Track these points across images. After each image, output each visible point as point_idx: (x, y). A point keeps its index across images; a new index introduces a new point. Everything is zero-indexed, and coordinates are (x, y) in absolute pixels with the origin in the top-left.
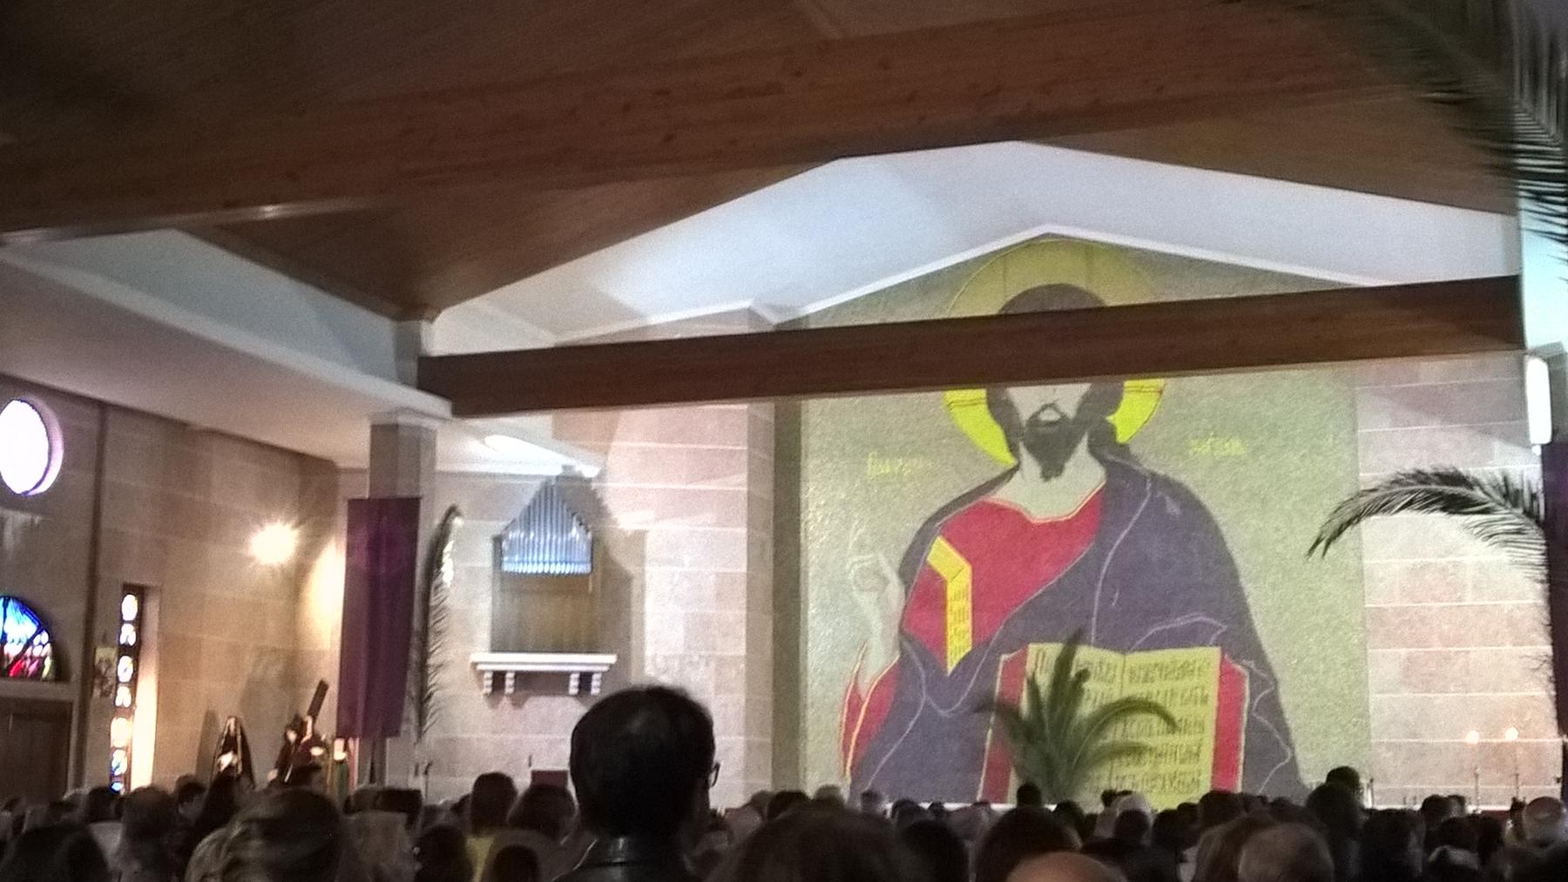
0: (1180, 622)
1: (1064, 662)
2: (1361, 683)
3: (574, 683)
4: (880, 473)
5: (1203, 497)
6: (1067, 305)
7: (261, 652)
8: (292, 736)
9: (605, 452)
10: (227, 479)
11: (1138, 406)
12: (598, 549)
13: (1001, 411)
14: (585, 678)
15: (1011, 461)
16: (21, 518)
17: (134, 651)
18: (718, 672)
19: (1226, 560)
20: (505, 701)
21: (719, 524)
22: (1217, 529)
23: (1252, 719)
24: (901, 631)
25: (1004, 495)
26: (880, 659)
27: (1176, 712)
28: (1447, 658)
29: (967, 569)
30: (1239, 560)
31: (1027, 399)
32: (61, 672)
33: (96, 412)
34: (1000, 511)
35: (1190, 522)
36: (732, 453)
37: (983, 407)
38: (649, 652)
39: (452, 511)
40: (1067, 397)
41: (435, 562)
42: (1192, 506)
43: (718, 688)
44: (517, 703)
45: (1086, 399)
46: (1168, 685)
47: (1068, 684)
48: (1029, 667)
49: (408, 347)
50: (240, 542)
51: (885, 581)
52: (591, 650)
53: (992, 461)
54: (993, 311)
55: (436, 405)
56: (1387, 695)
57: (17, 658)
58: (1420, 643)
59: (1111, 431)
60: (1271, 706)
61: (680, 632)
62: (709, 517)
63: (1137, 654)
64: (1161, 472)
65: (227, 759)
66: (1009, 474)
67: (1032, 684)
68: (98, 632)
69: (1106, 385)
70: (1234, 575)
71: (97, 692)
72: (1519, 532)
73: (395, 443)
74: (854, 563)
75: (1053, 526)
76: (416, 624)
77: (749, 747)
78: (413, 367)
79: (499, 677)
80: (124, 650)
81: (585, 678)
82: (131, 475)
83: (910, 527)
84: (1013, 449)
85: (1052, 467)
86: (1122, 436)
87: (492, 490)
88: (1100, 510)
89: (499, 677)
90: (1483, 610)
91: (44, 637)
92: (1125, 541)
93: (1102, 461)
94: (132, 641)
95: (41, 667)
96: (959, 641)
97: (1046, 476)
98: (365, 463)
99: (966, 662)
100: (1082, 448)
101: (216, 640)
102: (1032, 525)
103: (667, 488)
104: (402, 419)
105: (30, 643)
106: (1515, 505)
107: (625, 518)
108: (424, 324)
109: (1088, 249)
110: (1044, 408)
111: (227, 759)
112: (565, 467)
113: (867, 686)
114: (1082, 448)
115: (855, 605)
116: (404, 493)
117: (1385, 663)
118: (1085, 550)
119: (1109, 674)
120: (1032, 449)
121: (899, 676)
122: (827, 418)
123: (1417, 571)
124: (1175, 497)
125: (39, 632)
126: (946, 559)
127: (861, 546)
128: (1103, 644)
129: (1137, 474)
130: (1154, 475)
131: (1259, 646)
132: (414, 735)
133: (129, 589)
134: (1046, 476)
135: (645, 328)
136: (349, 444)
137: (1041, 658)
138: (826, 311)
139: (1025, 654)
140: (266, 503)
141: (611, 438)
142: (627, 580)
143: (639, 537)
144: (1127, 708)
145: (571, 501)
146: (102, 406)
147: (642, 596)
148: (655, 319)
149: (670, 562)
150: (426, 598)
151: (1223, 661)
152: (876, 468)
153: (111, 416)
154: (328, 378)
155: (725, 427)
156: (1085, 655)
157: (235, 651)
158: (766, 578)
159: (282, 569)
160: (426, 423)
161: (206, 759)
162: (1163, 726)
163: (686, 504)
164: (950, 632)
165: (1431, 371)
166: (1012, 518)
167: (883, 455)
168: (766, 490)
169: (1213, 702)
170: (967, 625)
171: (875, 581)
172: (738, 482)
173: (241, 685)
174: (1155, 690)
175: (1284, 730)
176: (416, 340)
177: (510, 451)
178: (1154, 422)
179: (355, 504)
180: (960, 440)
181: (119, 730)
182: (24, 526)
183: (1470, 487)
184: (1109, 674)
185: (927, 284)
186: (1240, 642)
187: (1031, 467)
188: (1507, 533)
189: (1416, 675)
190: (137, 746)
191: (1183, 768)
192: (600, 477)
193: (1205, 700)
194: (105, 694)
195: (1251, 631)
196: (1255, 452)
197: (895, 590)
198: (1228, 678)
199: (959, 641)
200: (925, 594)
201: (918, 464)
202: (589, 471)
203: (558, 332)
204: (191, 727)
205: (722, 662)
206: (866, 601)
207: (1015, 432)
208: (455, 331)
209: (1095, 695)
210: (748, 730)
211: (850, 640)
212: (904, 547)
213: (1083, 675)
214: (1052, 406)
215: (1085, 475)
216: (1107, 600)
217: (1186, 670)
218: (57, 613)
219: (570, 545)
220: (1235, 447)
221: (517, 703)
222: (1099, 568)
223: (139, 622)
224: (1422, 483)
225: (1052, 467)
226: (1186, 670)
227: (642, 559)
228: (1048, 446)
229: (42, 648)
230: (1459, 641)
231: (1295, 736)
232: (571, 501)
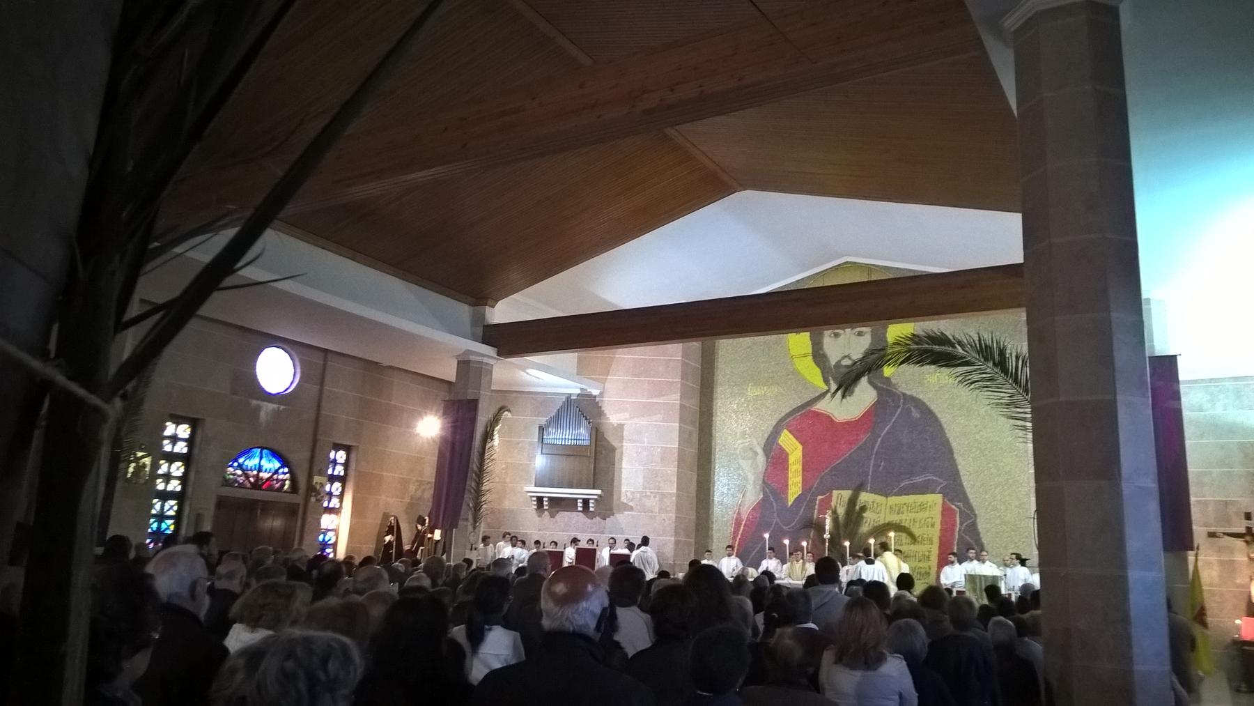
0: (919, 479)
1: (852, 501)
4: (760, 391)
5: (933, 407)
7: (421, 483)
12: (597, 434)
14: (586, 502)
15: (826, 388)
16: (272, 406)
17: (343, 480)
18: (661, 500)
19: (946, 444)
21: (664, 420)
22: (940, 425)
24: (764, 481)
25: (824, 406)
26: (753, 496)
27: (916, 531)
29: (800, 447)
30: (954, 444)
32: (294, 488)
33: (321, 354)
34: (817, 415)
38: (623, 490)
41: (488, 436)
43: (660, 509)
46: (913, 515)
47: (854, 514)
48: (833, 504)
49: (478, 319)
50: (409, 426)
51: (756, 453)
57: (268, 479)
61: (641, 480)
62: (659, 417)
63: (893, 498)
64: (909, 393)
65: (388, 538)
66: (823, 395)
67: (834, 512)
68: (316, 469)
70: (951, 452)
71: (313, 499)
72: (991, 380)
74: (740, 444)
75: (848, 423)
76: (474, 466)
77: (677, 543)
78: (480, 331)
79: (540, 500)
80: (333, 479)
81: (586, 502)
82: (342, 388)
83: (767, 426)
84: (826, 381)
87: (538, 399)
89: (540, 500)
91: (286, 470)
92: (888, 433)
93: (875, 387)
94: (342, 474)
95: (283, 485)
96: (795, 488)
99: (798, 500)
101: (391, 476)
103: (637, 398)
104: (472, 358)
105: (276, 472)
106: (986, 359)
107: (613, 417)
108: (487, 308)
110: (844, 357)
111: (388, 538)
118: (864, 438)
119: (878, 508)
121: (762, 505)
124: (916, 407)
125: (282, 467)
126: (787, 441)
129: (895, 394)
130: (904, 394)
131: (964, 493)
132: (470, 528)
133: (337, 447)
136: (449, 371)
137: (840, 498)
139: (831, 496)
140: (425, 405)
142: (614, 449)
145: (584, 409)
146: (325, 351)
147: (621, 460)
149: (634, 441)
150: (482, 454)
151: (944, 503)
153: (330, 356)
154: (435, 336)
156: (865, 497)
157: (404, 482)
158: (693, 451)
159: (434, 441)
160: (485, 360)
161: (380, 538)
162: (909, 540)
163: (647, 410)
164: (790, 482)
168: (694, 404)
169: (938, 526)
170: (799, 479)
171: (750, 454)
172: (675, 399)
173: (407, 500)
174: (905, 518)
176: (483, 316)
177: (547, 376)
181: (327, 521)
182: (273, 410)
183: (953, 346)
184: (878, 508)
186: (954, 491)
188: (983, 379)
190: (338, 529)
191: (921, 564)
192: (601, 394)
193: (933, 526)
194: (318, 501)
195: (961, 485)
197: (761, 459)
198: (946, 513)
199: (795, 488)
201: (775, 389)
202: (595, 392)
204: (373, 521)
205: (663, 496)
206: (746, 464)
208: (503, 312)
209: (871, 519)
210: (676, 534)
211: (735, 488)
212: (766, 436)
213: (863, 509)
214: (848, 357)
216: (877, 466)
217: (922, 507)
218: (292, 457)
222: (873, 448)
223: (346, 465)
224: (917, 343)
226: (922, 507)
227: (622, 438)
229: (284, 475)
232: (584, 409)
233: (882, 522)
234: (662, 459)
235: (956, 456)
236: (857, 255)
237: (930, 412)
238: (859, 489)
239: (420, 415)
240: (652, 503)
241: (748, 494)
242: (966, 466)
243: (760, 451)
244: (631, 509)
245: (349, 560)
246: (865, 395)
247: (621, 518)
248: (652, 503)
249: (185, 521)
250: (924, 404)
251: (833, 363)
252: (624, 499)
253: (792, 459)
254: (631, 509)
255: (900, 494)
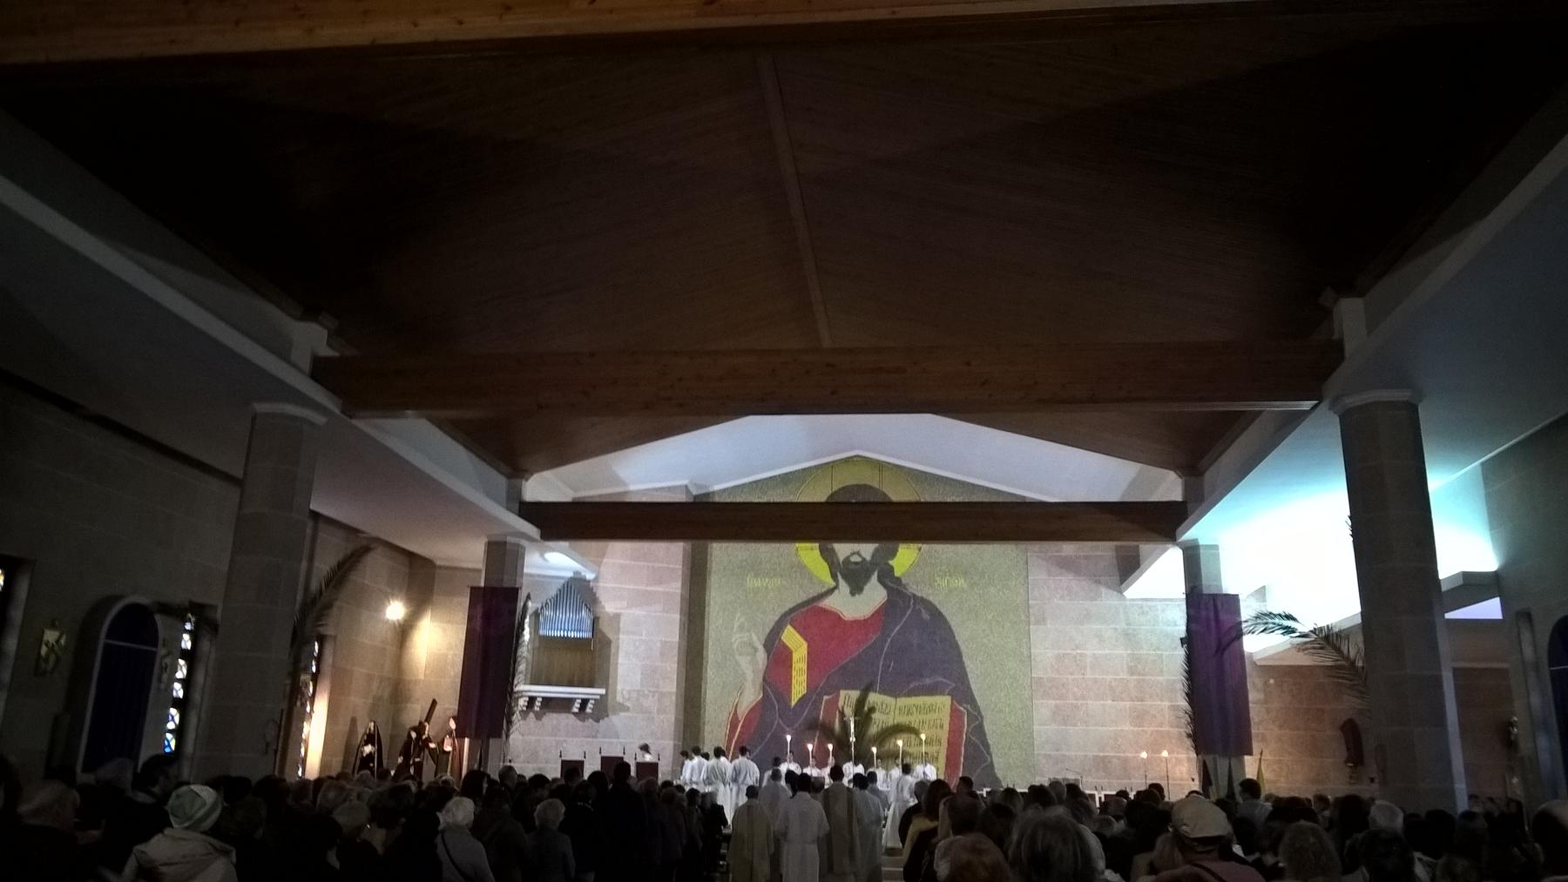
0: (928, 681)
1: (861, 702)
2: (1031, 718)
3: (577, 705)
4: (759, 587)
6: (860, 498)
8: (414, 735)
9: (599, 564)
10: (376, 566)
11: (905, 558)
13: (828, 555)
14: (584, 702)
15: (833, 584)
19: (955, 646)
20: (531, 715)
23: (969, 740)
25: (830, 603)
26: (751, 696)
28: (1076, 707)
29: (805, 645)
30: (963, 648)
31: (843, 550)
34: (825, 612)
35: (934, 623)
36: (673, 570)
37: (817, 552)
38: (619, 687)
39: (528, 597)
40: (867, 550)
42: (937, 615)
44: (538, 717)
45: (877, 550)
46: (921, 717)
47: (864, 715)
48: (840, 704)
51: (756, 650)
52: (591, 686)
53: (821, 583)
54: (823, 499)
55: (533, 531)
56: (1043, 728)
58: (1061, 697)
59: (892, 569)
60: (979, 730)
61: (639, 677)
65: (368, 749)
66: (831, 591)
69: (890, 545)
70: (960, 655)
73: (503, 555)
74: (737, 639)
75: (856, 622)
81: (584, 702)
84: (834, 577)
85: (856, 588)
86: (897, 574)
88: (886, 613)
90: (1096, 681)
92: (898, 633)
96: (799, 687)
97: (853, 594)
98: (481, 565)
99: (802, 700)
100: (874, 578)
101: (360, 672)
102: (845, 622)
103: (633, 591)
104: (510, 539)
107: (609, 606)
109: (880, 466)
111: (368, 749)
112: (576, 573)
113: (743, 711)
114: (874, 578)
115: (737, 663)
116: (506, 584)
117: (1043, 709)
119: (887, 709)
120: (845, 577)
121: (763, 706)
122: (724, 554)
123: (1059, 658)
126: (792, 638)
127: (741, 628)
128: (883, 692)
134: (853, 594)
135: (626, 493)
136: (469, 553)
137: (848, 698)
138: (724, 490)
141: (603, 555)
142: (608, 643)
143: (617, 616)
144: (898, 729)
145: (578, 593)
148: (632, 488)
149: (634, 633)
152: (752, 582)
153: (321, 525)
155: (670, 555)
156: (874, 698)
157: (370, 678)
163: (643, 599)
165: (1068, 549)
166: (835, 617)
167: (756, 575)
169: (946, 727)
173: (370, 701)
174: (913, 720)
175: (987, 746)
176: (520, 492)
177: (553, 563)
178: (915, 566)
179: (475, 591)
180: (802, 568)
184: (887, 709)
185: (785, 479)
186: (962, 694)
187: (844, 587)
189: (1063, 717)
195: (969, 688)
196: (972, 586)
197: (762, 656)
198: (955, 714)
199: (799, 687)
200: (779, 658)
201: (778, 581)
202: (590, 576)
203: (575, 490)
204: (343, 727)
205: (662, 695)
206: (744, 662)
207: (835, 567)
208: (543, 487)
209: (879, 721)
211: (735, 684)
213: (872, 710)
215: (874, 595)
217: (931, 709)
219: (581, 621)
220: (961, 582)
221: (538, 717)
225: (856, 588)
226: (931, 709)
227: (618, 631)
228: (855, 577)
230: (1083, 698)
231: (993, 749)
233: (890, 723)
234: (662, 654)
235: (965, 659)
236: (868, 450)
237: (940, 614)
238: (866, 691)
239: (394, 596)
240: (650, 703)
241: (746, 693)
242: (973, 667)
243: (761, 648)
244: (627, 709)
245: (319, 782)
246: (874, 595)
247: (616, 720)
248: (650, 703)
249: (191, 735)
250: (930, 603)
251: (841, 559)
252: (619, 699)
253: (795, 656)
254: (627, 709)
255: (910, 694)
